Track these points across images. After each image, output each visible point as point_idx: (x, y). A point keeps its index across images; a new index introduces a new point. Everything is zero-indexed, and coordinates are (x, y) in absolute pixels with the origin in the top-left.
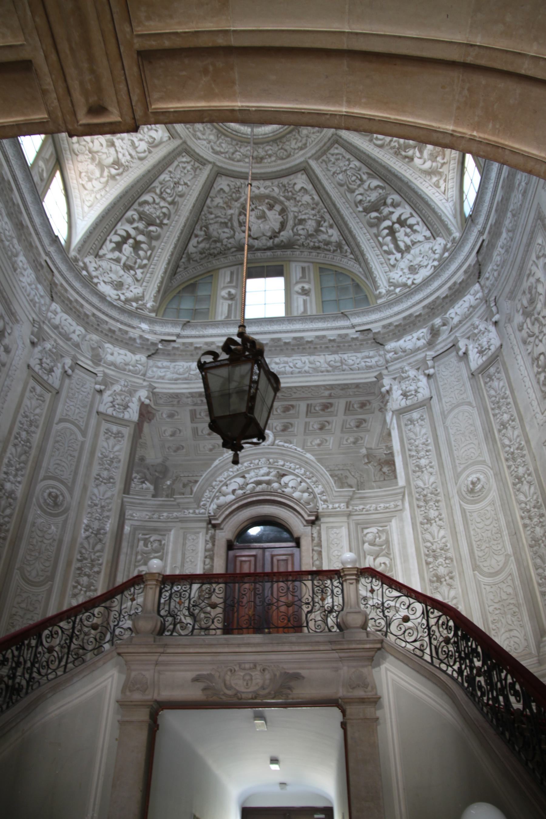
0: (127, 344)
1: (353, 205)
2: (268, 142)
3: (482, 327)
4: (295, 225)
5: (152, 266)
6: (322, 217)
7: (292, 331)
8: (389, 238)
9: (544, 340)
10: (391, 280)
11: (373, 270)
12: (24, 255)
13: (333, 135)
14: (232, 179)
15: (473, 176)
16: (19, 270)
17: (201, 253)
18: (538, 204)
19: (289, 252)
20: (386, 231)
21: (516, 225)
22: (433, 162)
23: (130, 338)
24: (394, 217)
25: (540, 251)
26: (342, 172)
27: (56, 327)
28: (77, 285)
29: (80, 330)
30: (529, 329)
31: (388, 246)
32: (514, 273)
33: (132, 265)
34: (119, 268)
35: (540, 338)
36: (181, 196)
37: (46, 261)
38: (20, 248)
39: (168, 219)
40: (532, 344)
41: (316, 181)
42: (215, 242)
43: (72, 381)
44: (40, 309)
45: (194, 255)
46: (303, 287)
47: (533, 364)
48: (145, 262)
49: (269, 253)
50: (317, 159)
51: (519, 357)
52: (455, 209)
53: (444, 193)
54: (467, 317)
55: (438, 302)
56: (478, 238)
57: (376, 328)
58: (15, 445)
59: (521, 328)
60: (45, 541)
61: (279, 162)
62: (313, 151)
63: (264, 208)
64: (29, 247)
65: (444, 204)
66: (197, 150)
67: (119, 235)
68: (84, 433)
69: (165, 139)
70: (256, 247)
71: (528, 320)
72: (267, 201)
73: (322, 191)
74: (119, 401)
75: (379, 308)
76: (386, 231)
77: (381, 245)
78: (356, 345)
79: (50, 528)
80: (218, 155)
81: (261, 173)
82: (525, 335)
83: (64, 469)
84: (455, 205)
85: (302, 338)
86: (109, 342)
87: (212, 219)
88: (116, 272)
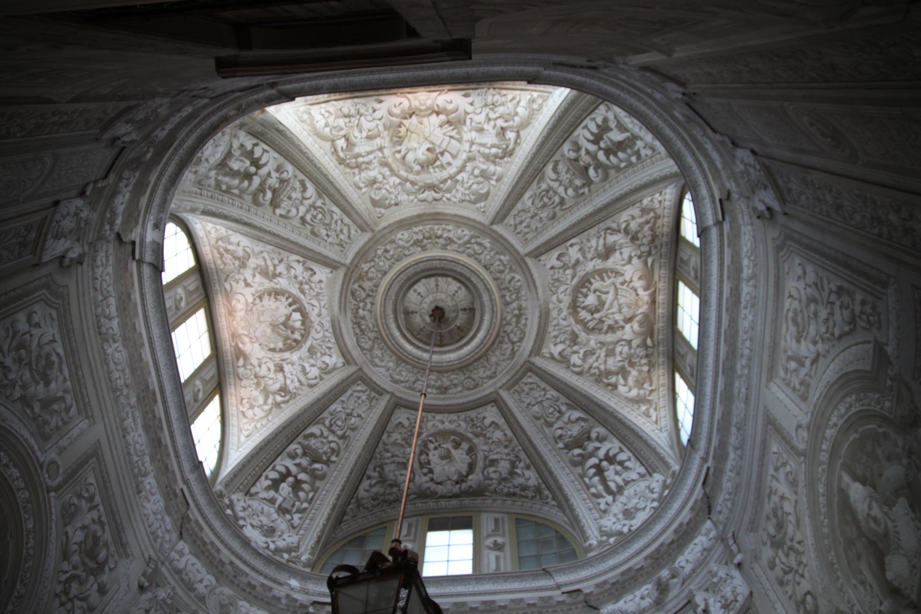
0: (268, 603)
1: (552, 441)
2: (453, 370)
3: (722, 573)
4: (486, 467)
5: (313, 511)
6: (517, 456)
7: (480, 594)
8: (596, 479)
9: (806, 575)
10: (603, 529)
11: (581, 518)
13: (525, 362)
15: (686, 398)
16: (144, 493)
17: (374, 499)
18: (765, 407)
19: (479, 500)
20: (593, 471)
21: (743, 440)
22: (640, 389)
23: (274, 597)
24: (592, 148)
25: (778, 461)
26: (537, 403)
27: (179, 572)
28: (217, 524)
29: (209, 579)
30: (783, 563)
31: (596, 487)
32: (751, 498)
33: (289, 508)
34: (272, 510)
35: (800, 572)
36: (353, 429)
37: (182, 490)
38: (151, 468)
39: (337, 456)
40: (791, 583)
41: (508, 414)
42: (391, 486)
44: (161, 545)
45: (365, 501)
46: (495, 541)
47: (798, 610)
48: (305, 505)
49: (455, 502)
50: (508, 389)
51: (778, 605)
52: (671, 440)
53: (656, 423)
54: (701, 563)
55: (663, 549)
56: (701, 466)
57: (587, 587)
59: (772, 565)
61: (466, 392)
62: (504, 381)
63: (449, 446)
64: (164, 471)
65: (659, 437)
66: (374, 379)
67: (277, 471)
69: (339, 365)
71: (780, 553)
72: (452, 438)
73: (515, 425)
75: (589, 563)
77: (588, 487)
78: (562, 610)
81: (446, 406)
82: (780, 573)
84: (670, 435)
85: (493, 602)
86: (245, 599)
87: (388, 458)
88: (269, 515)
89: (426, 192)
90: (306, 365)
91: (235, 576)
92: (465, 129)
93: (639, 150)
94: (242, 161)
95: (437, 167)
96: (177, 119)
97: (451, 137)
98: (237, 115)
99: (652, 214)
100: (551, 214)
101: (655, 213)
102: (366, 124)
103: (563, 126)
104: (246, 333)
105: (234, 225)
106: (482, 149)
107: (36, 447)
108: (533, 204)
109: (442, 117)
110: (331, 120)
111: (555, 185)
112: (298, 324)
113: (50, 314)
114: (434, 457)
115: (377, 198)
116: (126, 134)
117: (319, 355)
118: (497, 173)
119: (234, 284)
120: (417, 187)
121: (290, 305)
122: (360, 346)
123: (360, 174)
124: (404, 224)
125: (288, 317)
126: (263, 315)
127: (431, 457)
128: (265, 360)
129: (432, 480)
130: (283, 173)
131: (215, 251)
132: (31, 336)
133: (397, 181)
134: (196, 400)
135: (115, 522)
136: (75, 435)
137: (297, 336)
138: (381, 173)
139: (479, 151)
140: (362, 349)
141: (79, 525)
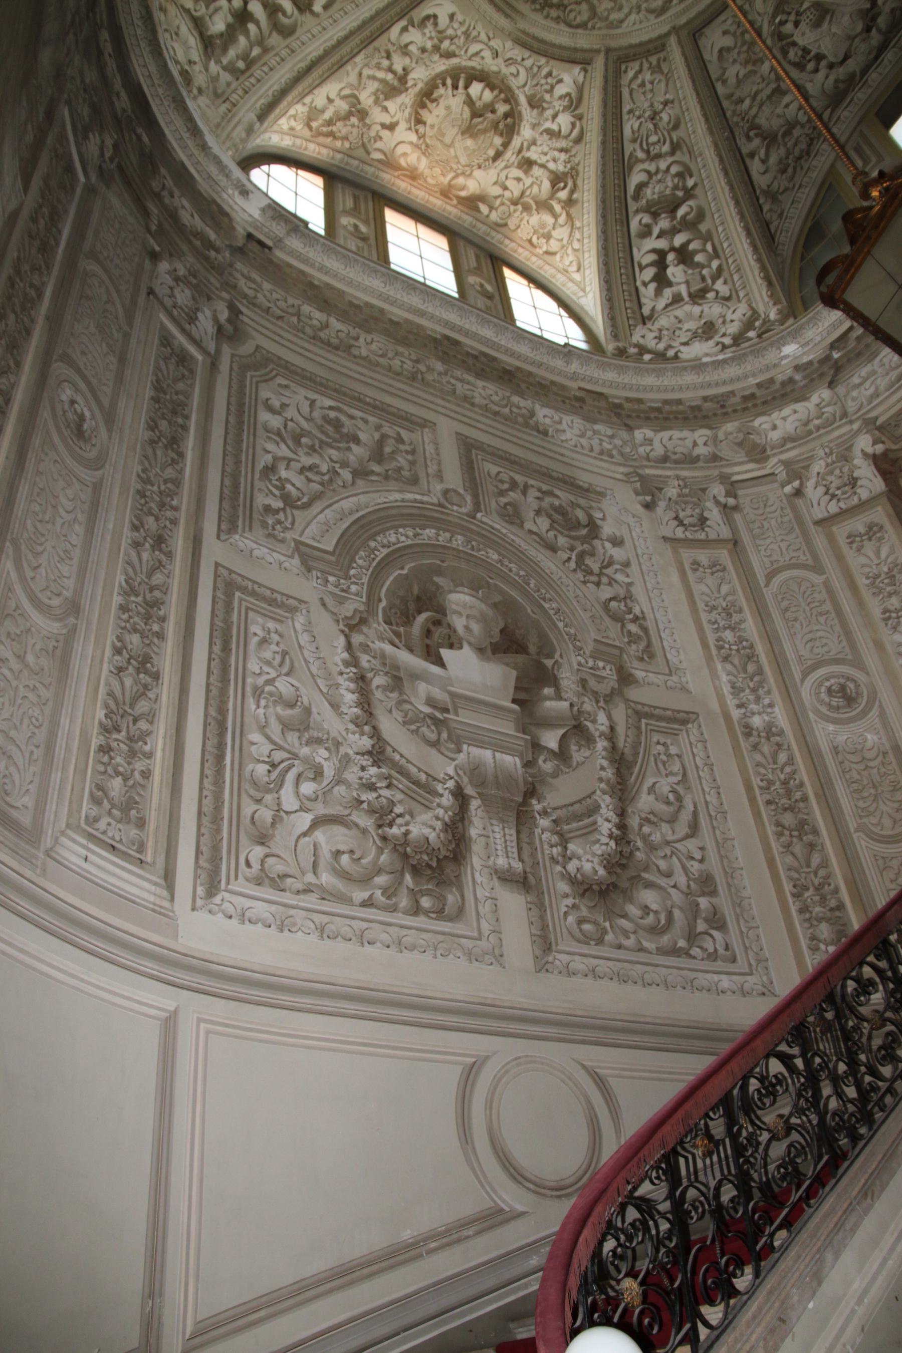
0: (783, 395)
5: (730, 261)
12: (543, 406)
14: (722, 18)
16: (551, 430)
17: (783, 171)
23: (783, 384)
27: (665, 459)
29: (701, 435)
33: (702, 285)
34: (687, 308)
36: (676, 126)
37: (580, 389)
38: (529, 402)
42: (788, 133)
43: (745, 512)
45: (775, 186)
48: (715, 264)
58: (726, 659)
60: (872, 764)
66: (635, 40)
67: (647, 266)
68: (818, 568)
70: (858, 70)
74: (836, 483)
79: (866, 740)
80: (668, 9)
83: (824, 641)
87: (750, 107)
88: (690, 316)
90: (548, 125)
91: (723, 406)
94: (216, 10)
96: (111, 65)
104: (452, 174)
105: (300, 88)
107: (418, 497)
112: (488, 96)
113: (280, 385)
114: (805, 37)
116: (102, 150)
117: (547, 97)
119: (379, 145)
121: (455, 87)
122: (577, 27)
125: (469, 102)
126: (443, 135)
127: (801, 42)
128: (503, 176)
129: (831, 66)
131: (321, 139)
132: (292, 420)
134: (490, 297)
135: (558, 479)
136: (432, 451)
137: (502, 108)
140: (583, 26)
141: (532, 514)
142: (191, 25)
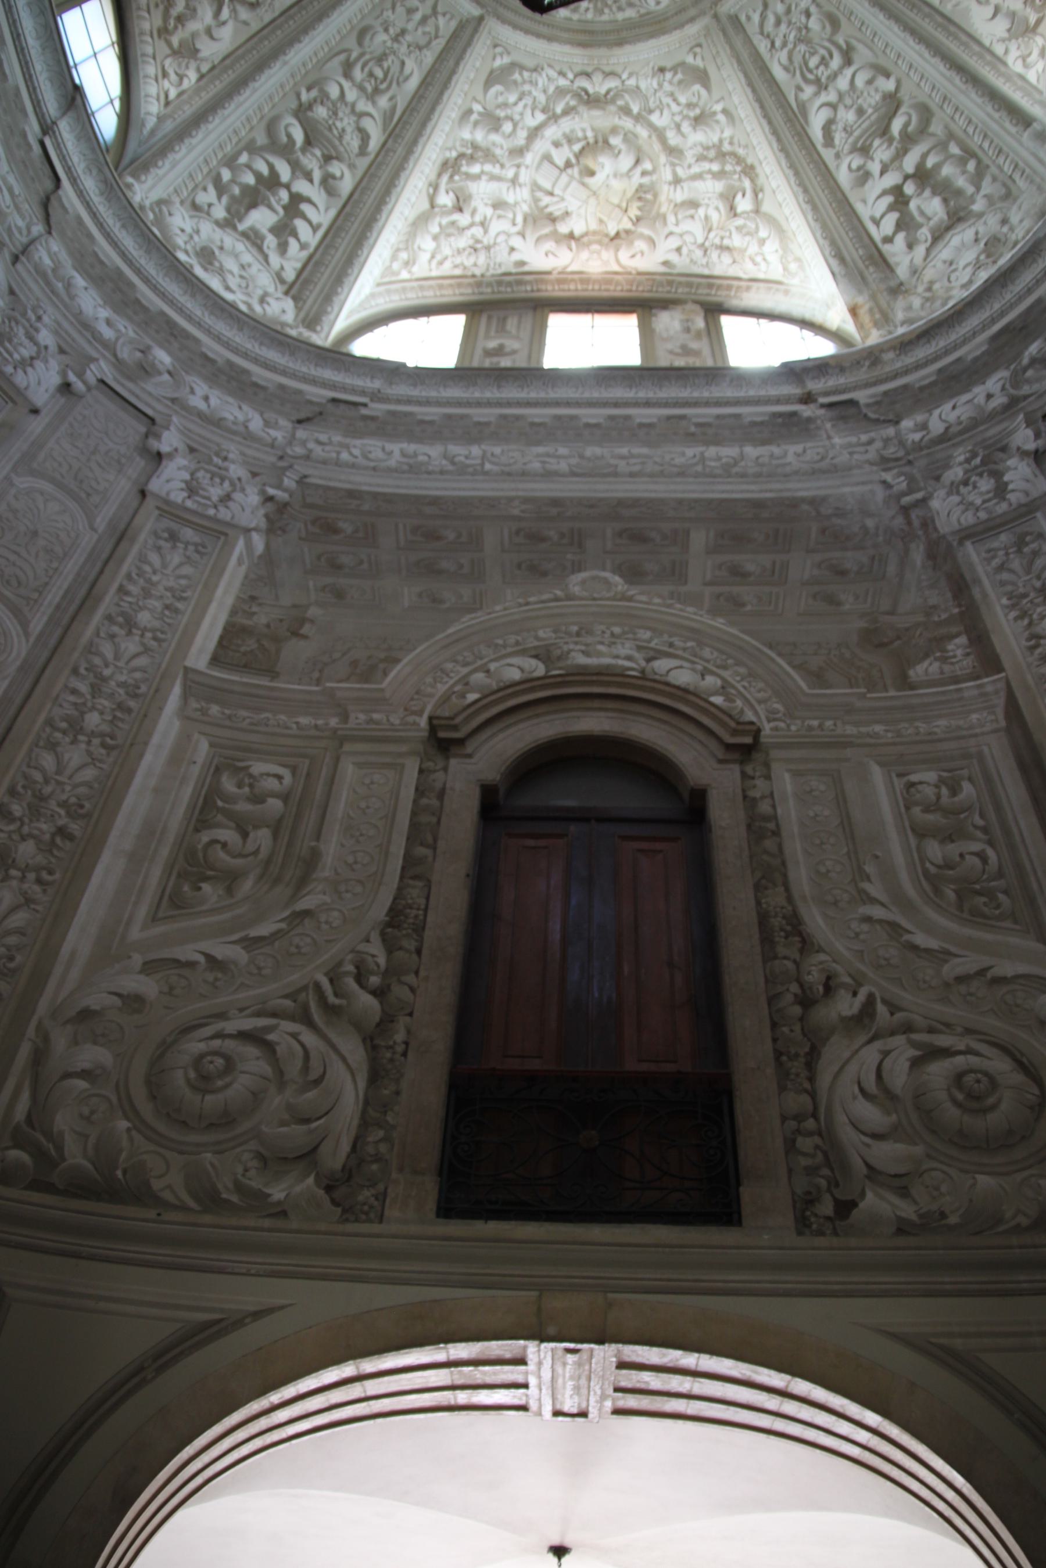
20: (265, 171)
24: (301, 186)
76: (265, 171)
89: (603, 91)
92: (525, 208)
93: (219, 197)
94: (922, 213)
95: (579, 140)
97: (551, 194)
98: (882, 351)
99: (175, 41)
100: (367, 41)
101: (169, 44)
102: (695, 229)
103: (355, 226)
106: (496, 170)
108: (403, 63)
109: (563, 229)
110: (753, 249)
111: (363, 106)
115: (697, 87)
118: (470, 126)
120: (620, 103)
123: (721, 141)
124: (652, 26)
130: (859, 169)
133: (654, 118)
138: (683, 136)
139: (502, 166)
142: (941, 245)
